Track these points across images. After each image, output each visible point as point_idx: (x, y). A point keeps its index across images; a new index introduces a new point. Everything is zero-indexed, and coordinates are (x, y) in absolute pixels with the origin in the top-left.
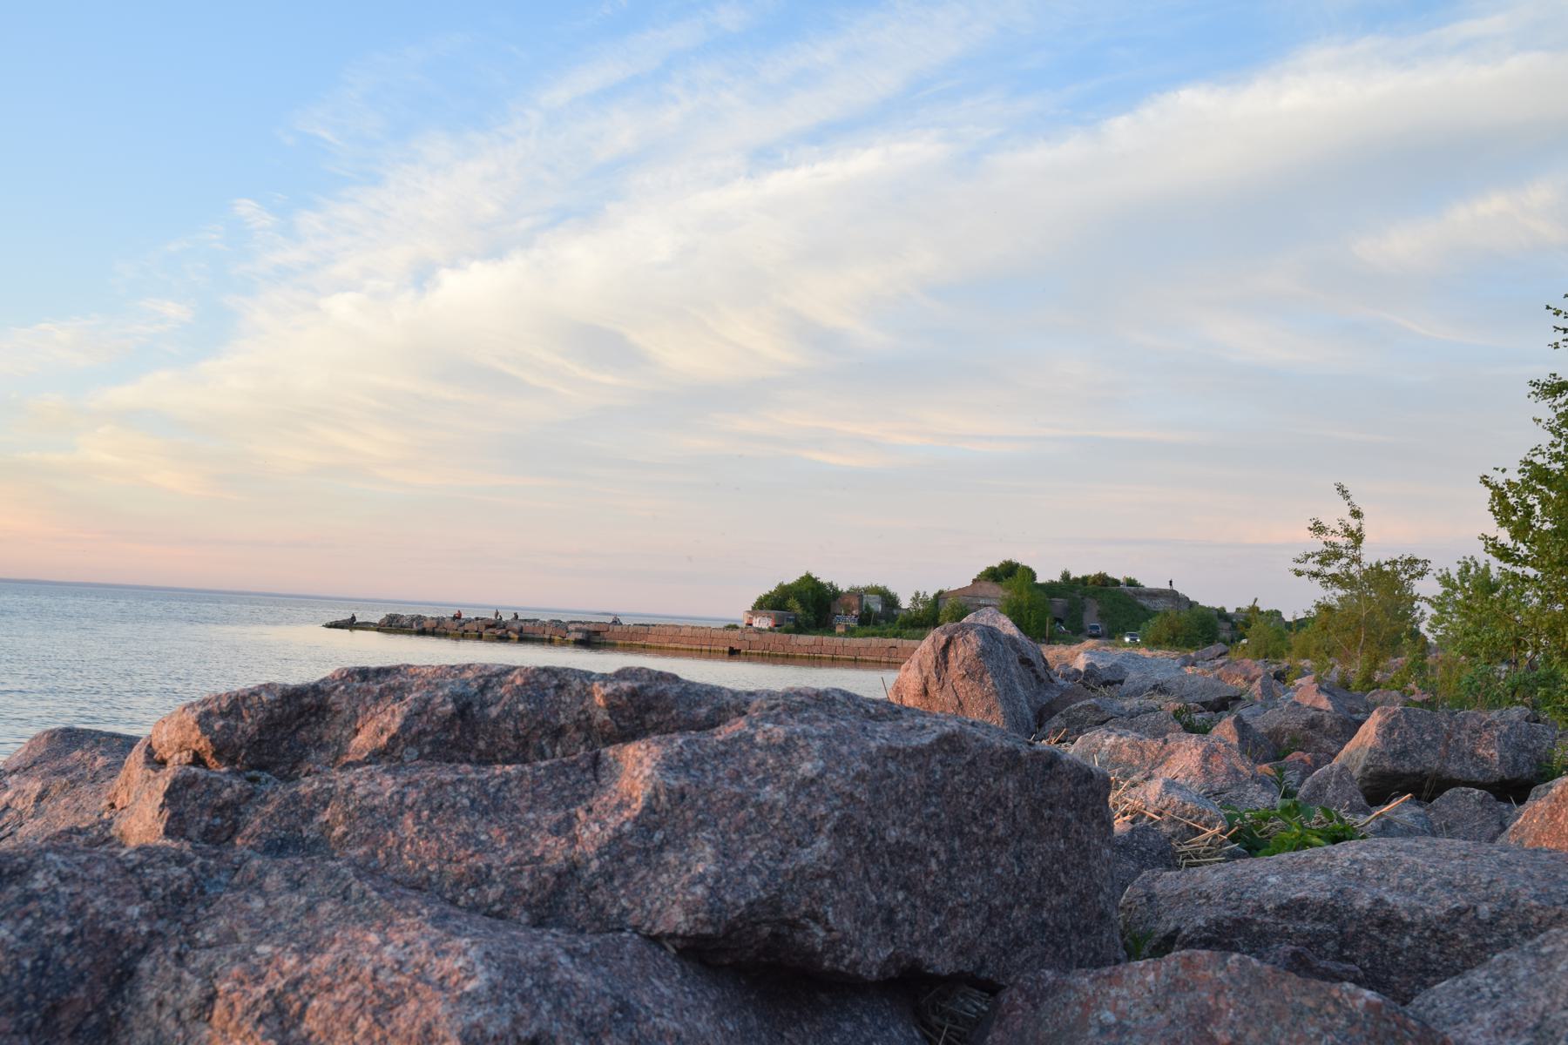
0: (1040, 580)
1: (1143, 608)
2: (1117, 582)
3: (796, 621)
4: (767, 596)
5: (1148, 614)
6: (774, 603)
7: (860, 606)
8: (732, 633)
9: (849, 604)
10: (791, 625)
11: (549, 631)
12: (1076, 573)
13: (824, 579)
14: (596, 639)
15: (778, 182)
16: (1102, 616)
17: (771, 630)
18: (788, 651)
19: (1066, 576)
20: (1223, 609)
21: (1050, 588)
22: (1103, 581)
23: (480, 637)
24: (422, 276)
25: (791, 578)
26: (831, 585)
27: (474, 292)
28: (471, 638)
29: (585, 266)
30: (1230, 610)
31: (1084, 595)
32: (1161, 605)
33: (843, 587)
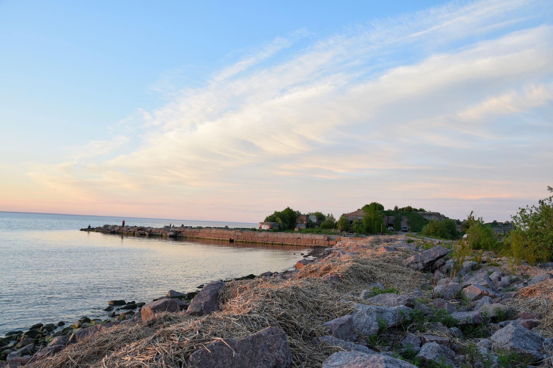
0: (385, 209)
1: (426, 220)
2: (416, 210)
3: (279, 226)
4: (270, 216)
5: (427, 222)
6: (271, 220)
7: (307, 220)
8: (226, 232)
9: (302, 219)
10: (277, 228)
11: (161, 231)
12: (400, 207)
13: (295, 209)
14: (179, 235)
15: (287, 98)
16: (408, 223)
17: (268, 231)
18: (254, 241)
19: (396, 208)
20: (376, 207)
21: (389, 213)
22: (409, 209)
23: (134, 235)
24: (193, 126)
25: (281, 209)
26: (298, 212)
27: (207, 131)
28: (130, 235)
29: (238, 122)
30: (461, 220)
31: (402, 215)
32: (433, 218)
33: (302, 213)
